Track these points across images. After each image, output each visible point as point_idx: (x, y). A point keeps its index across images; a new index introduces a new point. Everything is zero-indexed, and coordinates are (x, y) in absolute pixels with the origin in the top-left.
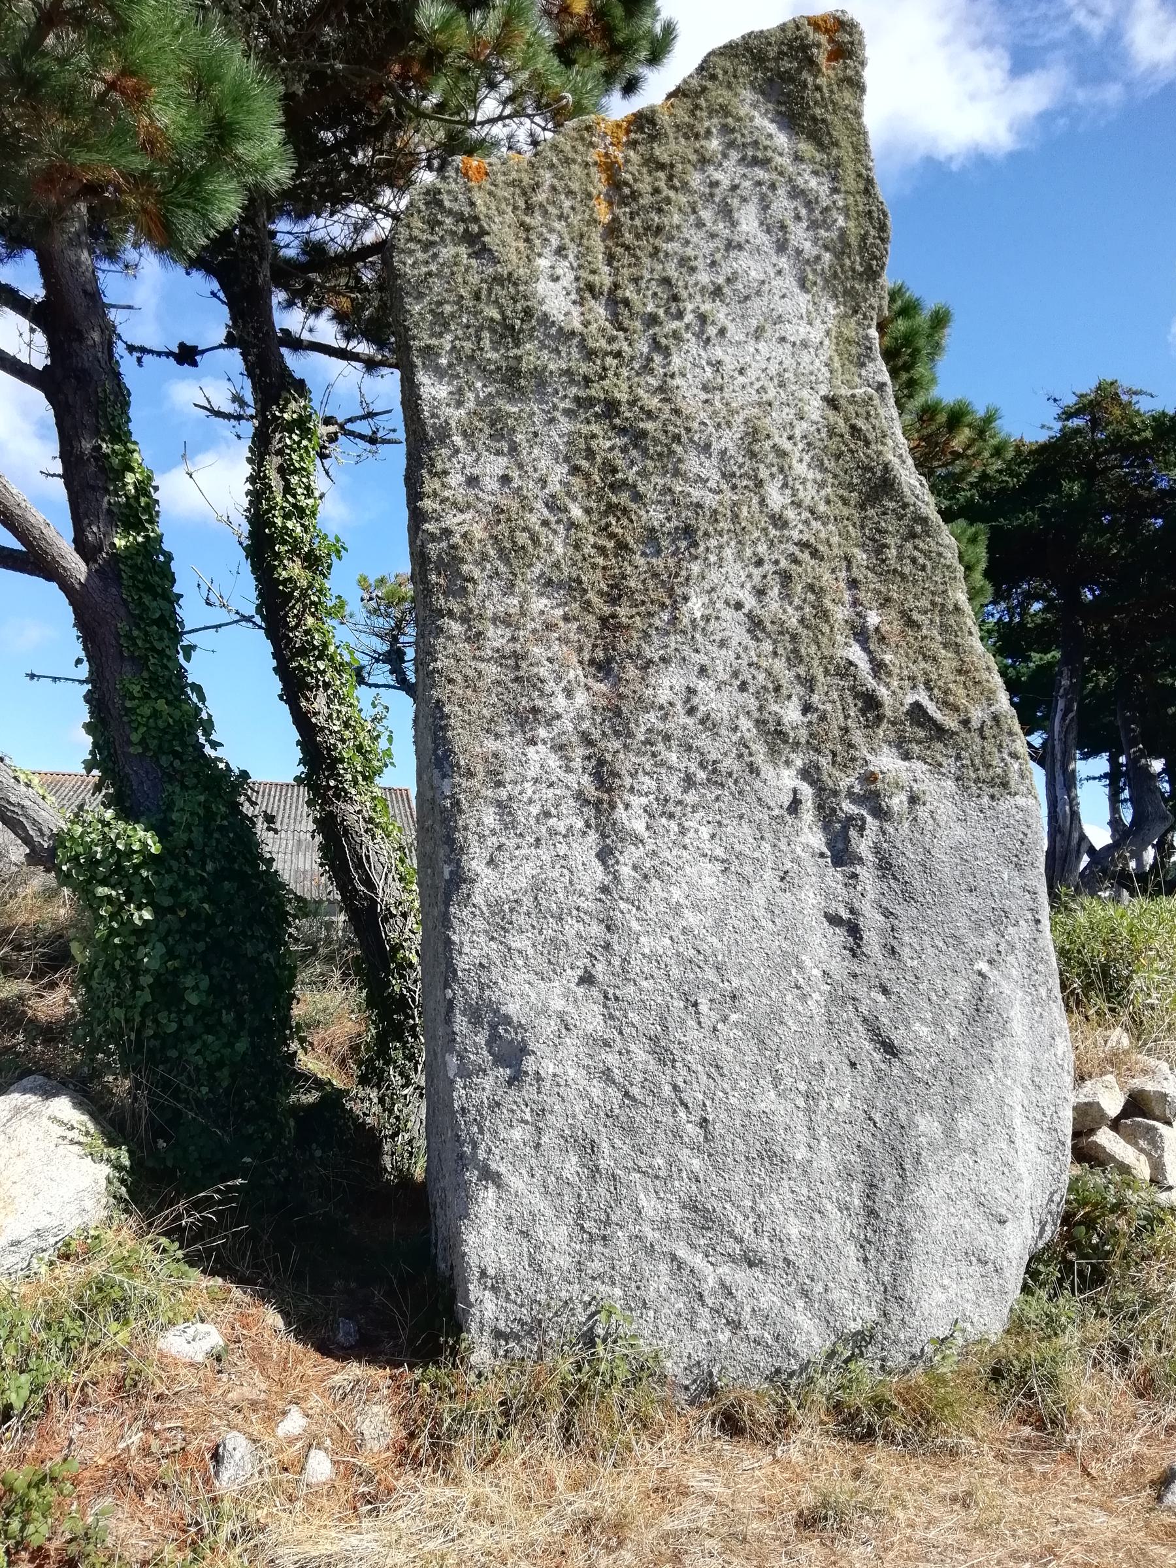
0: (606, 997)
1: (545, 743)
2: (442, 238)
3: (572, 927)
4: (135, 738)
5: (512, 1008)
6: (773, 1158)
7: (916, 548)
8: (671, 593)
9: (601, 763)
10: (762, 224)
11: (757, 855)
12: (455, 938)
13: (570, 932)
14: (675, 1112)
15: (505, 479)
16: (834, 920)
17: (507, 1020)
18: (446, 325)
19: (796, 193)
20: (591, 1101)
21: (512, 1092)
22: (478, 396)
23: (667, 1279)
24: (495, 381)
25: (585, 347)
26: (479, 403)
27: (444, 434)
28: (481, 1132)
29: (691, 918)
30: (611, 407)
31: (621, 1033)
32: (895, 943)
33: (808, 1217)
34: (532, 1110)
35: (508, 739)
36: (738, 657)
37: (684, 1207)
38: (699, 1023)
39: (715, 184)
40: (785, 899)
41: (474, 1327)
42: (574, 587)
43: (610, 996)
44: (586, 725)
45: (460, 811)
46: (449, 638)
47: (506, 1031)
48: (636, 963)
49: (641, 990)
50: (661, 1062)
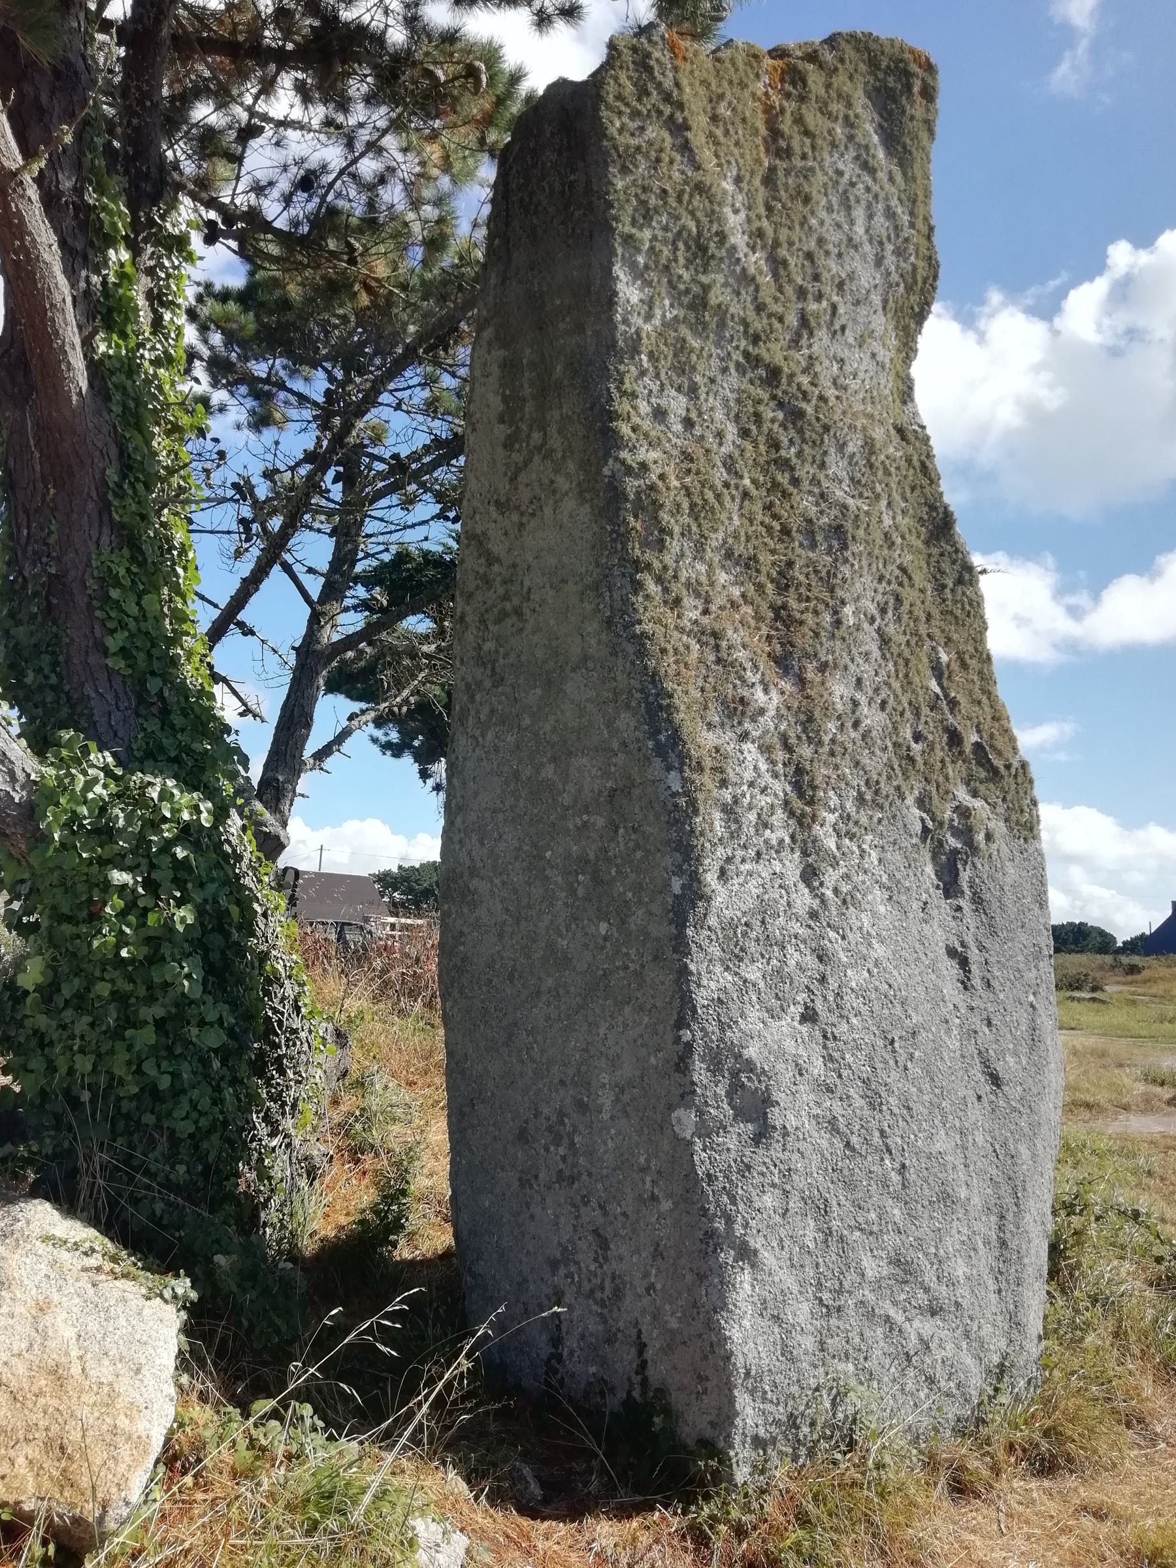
0: (825, 1037)
1: (753, 742)
3: (793, 957)
4: (113, 643)
5: (752, 1052)
6: (946, 1198)
7: (964, 594)
8: (832, 590)
9: (799, 771)
10: (867, 231)
12: (692, 967)
14: (882, 1159)
15: (688, 423)
16: (951, 952)
17: (750, 1066)
18: (647, 217)
19: (890, 214)
20: (823, 1156)
21: (761, 1152)
22: (664, 316)
23: (882, 1344)
24: (681, 305)
25: (756, 298)
26: (664, 324)
27: (635, 350)
28: (734, 1202)
29: (879, 951)
30: (774, 374)
32: (988, 976)
35: (719, 731)
39: (840, 173)
41: (737, 1439)
42: (750, 563)
45: (696, 812)
46: (647, 597)
47: (750, 1079)
48: (850, 1000)
50: (872, 1106)
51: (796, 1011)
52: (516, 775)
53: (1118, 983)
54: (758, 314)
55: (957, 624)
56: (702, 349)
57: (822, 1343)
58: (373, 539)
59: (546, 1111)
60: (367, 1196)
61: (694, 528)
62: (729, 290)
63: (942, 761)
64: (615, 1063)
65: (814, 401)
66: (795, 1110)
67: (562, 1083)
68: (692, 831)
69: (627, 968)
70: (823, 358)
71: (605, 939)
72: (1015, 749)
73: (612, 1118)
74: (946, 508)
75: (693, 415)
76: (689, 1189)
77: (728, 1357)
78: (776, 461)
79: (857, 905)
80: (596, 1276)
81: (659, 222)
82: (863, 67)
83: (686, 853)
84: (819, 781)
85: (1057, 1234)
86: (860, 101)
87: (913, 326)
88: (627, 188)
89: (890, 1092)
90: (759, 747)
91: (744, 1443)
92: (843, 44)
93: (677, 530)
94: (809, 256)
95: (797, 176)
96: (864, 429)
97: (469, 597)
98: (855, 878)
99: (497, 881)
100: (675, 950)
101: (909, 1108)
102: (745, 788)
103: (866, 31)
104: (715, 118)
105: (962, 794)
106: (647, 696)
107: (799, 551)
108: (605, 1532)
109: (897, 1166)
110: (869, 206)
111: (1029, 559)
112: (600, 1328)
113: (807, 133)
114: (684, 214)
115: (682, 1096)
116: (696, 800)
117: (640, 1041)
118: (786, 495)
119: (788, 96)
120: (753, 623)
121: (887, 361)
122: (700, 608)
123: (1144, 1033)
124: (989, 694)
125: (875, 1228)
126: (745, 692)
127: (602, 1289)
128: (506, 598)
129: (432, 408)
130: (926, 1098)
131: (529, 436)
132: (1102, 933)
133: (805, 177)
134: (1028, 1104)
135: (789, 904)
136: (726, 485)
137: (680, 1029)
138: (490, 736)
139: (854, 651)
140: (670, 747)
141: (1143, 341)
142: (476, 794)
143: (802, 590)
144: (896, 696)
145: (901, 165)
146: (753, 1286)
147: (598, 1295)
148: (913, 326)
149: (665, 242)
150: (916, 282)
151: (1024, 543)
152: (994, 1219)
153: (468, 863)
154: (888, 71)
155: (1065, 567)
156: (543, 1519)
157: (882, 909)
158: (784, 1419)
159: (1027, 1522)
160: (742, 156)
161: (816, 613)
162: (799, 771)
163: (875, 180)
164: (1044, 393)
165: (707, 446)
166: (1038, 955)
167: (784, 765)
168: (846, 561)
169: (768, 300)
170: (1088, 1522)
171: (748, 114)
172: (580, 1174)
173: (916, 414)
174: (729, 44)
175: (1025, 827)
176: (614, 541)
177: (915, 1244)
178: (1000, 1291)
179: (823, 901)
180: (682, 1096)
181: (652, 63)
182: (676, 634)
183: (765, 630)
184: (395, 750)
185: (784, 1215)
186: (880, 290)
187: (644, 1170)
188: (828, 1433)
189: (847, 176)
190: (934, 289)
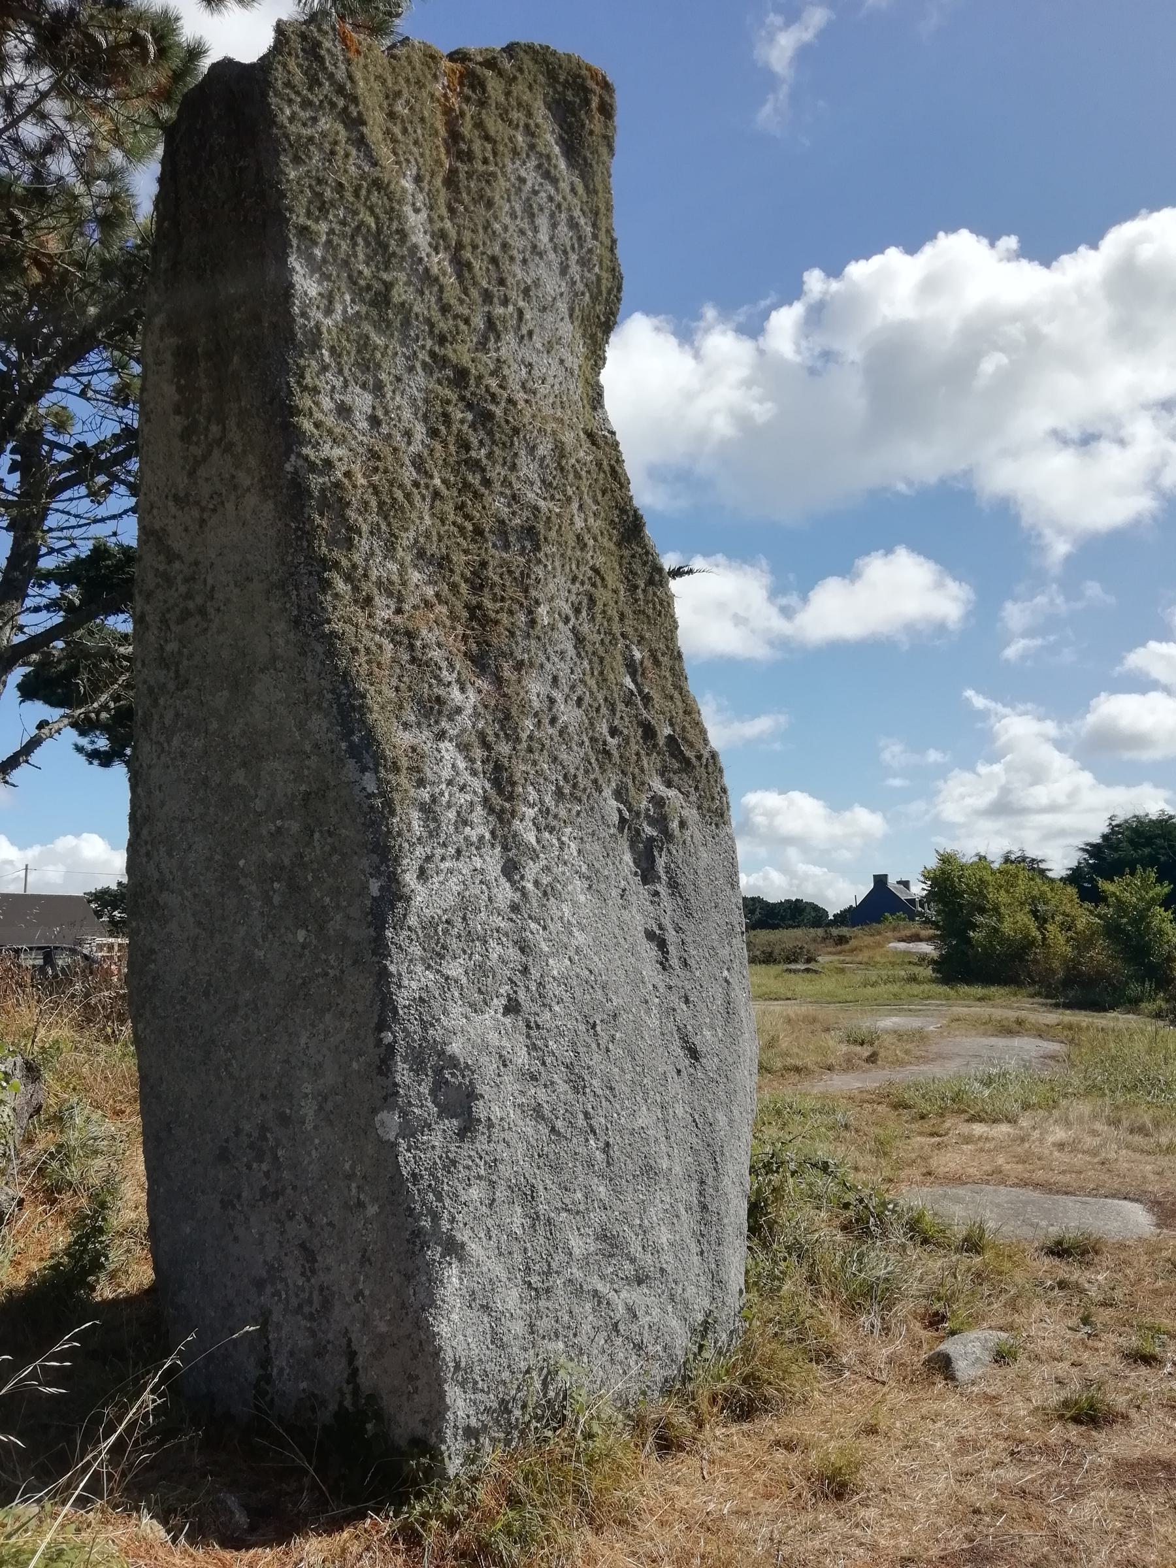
0: (528, 1026)
1: (451, 741)
2: (321, 102)
3: (495, 951)
5: (455, 1047)
6: (649, 1171)
7: (655, 594)
8: (526, 591)
9: (498, 768)
10: (551, 240)
12: (392, 968)
13: (494, 956)
14: (587, 1140)
15: (374, 421)
16: (650, 935)
17: (453, 1062)
19: (573, 224)
20: (528, 1143)
21: (466, 1146)
22: (345, 311)
23: (590, 1318)
24: (363, 301)
25: (440, 299)
26: (345, 319)
27: (315, 345)
28: (440, 1198)
29: (580, 938)
30: (461, 377)
31: (544, 1064)
33: (667, 1232)
35: (415, 730)
36: (572, 673)
37: (597, 1239)
38: (599, 1045)
39: (523, 181)
40: (626, 915)
42: (443, 563)
43: (532, 1024)
45: (393, 813)
46: (337, 596)
48: (553, 989)
50: (576, 1090)
51: (499, 1003)
52: (205, 782)
53: (830, 953)
54: (443, 315)
55: (649, 623)
56: (387, 347)
57: (531, 1325)
58: (55, 534)
59: (247, 1127)
60: (62, 1239)
61: (384, 527)
62: (412, 288)
63: (638, 754)
64: (317, 1071)
65: (503, 404)
66: (499, 1102)
67: (263, 1097)
68: (389, 832)
69: (327, 974)
70: (511, 362)
71: (304, 946)
72: (706, 741)
73: (316, 1128)
74: (635, 511)
75: (380, 413)
76: (393, 1190)
77: (437, 1352)
78: (466, 462)
79: (558, 896)
80: (303, 1290)
81: (335, 216)
82: (542, 79)
83: (383, 853)
84: (518, 776)
85: (759, 1191)
86: (541, 113)
87: (600, 335)
88: (300, 178)
89: (593, 1074)
90: (457, 746)
91: (455, 1435)
92: (522, 54)
93: (365, 528)
94: (494, 260)
95: (479, 180)
96: (554, 433)
97: (149, 596)
98: (555, 870)
99: (188, 894)
100: (374, 953)
101: (611, 1089)
102: (444, 786)
103: (544, 44)
104: (392, 115)
105: (657, 785)
106: (339, 696)
107: (493, 551)
108: (313, 1548)
109: (601, 1145)
110: (552, 216)
111: (745, 561)
112: (310, 1342)
113: (487, 138)
114: (362, 209)
115: (385, 1099)
116: (392, 800)
117: (342, 1047)
118: (477, 496)
119: (467, 99)
120: (448, 623)
121: (576, 367)
122: (393, 607)
123: (850, 998)
124: (680, 689)
125: (582, 1208)
126: (441, 691)
127: (310, 1302)
128: (189, 596)
129: (120, 396)
130: (628, 1077)
131: (207, 429)
132: (815, 908)
133: (488, 182)
134: (725, 1073)
135: (490, 899)
136: (416, 484)
137: (381, 1031)
138: (175, 742)
139: (550, 650)
140: (366, 749)
141: (837, 362)
142: (162, 804)
143: (497, 590)
144: (591, 693)
145: (582, 176)
146: (461, 1279)
147: (306, 1310)
148: (600, 335)
149: (343, 236)
150: (600, 292)
151: (737, 543)
152: (694, 1185)
153: (156, 875)
154: (566, 85)
155: (777, 570)
156: (248, 1548)
157: (582, 898)
158: (495, 1405)
159: (727, 1465)
160: (422, 155)
161: (511, 613)
162: (498, 768)
163: (557, 189)
164: (755, 408)
165: (395, 444)
166: (731, 933)
167: (483, 762)
168: (539, 562)
169: (453, 302)
170: (780, 1455)
171: (426, 114)
172: (284, 1188)
173: (606, 420)
174: (405, 41)
175: (716, 812)
176: (299, 538)
177: (620, 1218)
178: (702, 1253)
179: (524, 893)
180: (385, 1099)
181: (323, 52)
182: (367, 633)
183: (460, 630)
184: (104, 759)
185: (491, 1205)
186: (566, 298)
187: (350, 1177)
188: (539, 1412)
189: (529, 184)
190: (619, 300)
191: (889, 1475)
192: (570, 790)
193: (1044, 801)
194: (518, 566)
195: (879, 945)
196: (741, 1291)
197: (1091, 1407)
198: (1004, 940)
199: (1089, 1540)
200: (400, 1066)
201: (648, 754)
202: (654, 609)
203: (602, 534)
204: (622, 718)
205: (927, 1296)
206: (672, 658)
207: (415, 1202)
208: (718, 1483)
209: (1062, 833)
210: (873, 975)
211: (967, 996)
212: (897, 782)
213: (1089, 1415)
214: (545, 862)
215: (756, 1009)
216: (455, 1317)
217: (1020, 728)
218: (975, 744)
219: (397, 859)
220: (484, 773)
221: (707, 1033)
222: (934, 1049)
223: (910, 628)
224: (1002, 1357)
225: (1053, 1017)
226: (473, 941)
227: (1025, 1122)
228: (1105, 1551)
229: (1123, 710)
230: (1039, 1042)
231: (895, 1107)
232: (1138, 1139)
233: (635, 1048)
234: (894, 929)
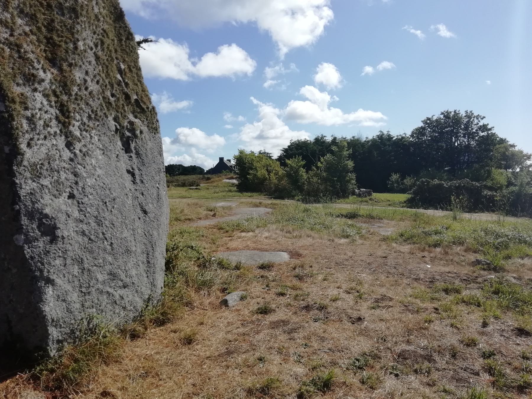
0: (79, 203)
1: (40, 92)
3: (63, 176)
5: (47, 211)
6: (128, 251)
7: (129, 43)
8: (73, 34)
11: (110, 148)
12: (17, 181)
13: (63, 178)
14: (104, 242)
16: (128, 172)
17: (46, 216)
21: (53, 246)
23: (106, 300)
28: (43, 264)
31: (85, 216)
33: (134, 269)
34: (62, 251)
36: (94, 70)
40: (118, 164)
41: (50, 343)
44: (54, 87)
45: (13, 120)
47: (47, 221)
48: (88, 190)
49: (89, 199)
50: (99, 225)
51: (66, 195)
55: (127, 55)
57: (82, 305)
63: (123, 105)
66: (67, 229)
72: (150, 102)
84: (71, 109)
89: (105, 219)
90: (43, 95)
98: (88, 146)
101: (113, 224)
102: (37, 111)
105: (131, 117)
107: (57, 16)
109: (109, 243)
120: (37, 43)
122: (9, 33)
125: (102, 265)
126: (34, 72)
135: (60, 156)
139: (84, 60)
143: (59, 32)
144: (103, 80)
146: (53, 292)
151: (177, 36)
152: (145, 255)
155: (191, 47)
157: (100, 157)
158: (69, 331)
161: (66, 43)
167: (55, 102)
170: (172, 335)
175: (154, 129)
178: (148, 277)
179: (75, 154)
183: (43, 47)
191: (206, 335)
192: (94, 116)
193: (274, 135)
194: (69, 24)
195: (220, 180)
196: (162, 288)
197: (265, 309)
198: (258, 178)
199: (260, 344)
200: (23, 218)
201: (127, 105)
202: (129, 49)
203: (107, 16)
204: (116, 90)
205: (222, 284)
206: (137, 69)
207: (32, 266)
208: (153, 345)
209: (278, 145)
210: (217, 190)
211: (246, 196)
212: (228, 127)
213: (265, 311)
214: (84, 143)
215: (172, 200)
216: (51, 304)
217: (268, 110)
218: (254, 116)
219: (17, 139)
220: (56, 107)
221: (150, 205)
222: (234, 212)
223: (235, 74)
224: (242, 298)
225: (270, 202)
226: (53, 172)
227: (257, 232)
228: (264, 345)
229: (297, 106)
230: (265, 209)
231: (219, 229)
232: (288, 235)
233: (122, 210)
234: (225, 175)
